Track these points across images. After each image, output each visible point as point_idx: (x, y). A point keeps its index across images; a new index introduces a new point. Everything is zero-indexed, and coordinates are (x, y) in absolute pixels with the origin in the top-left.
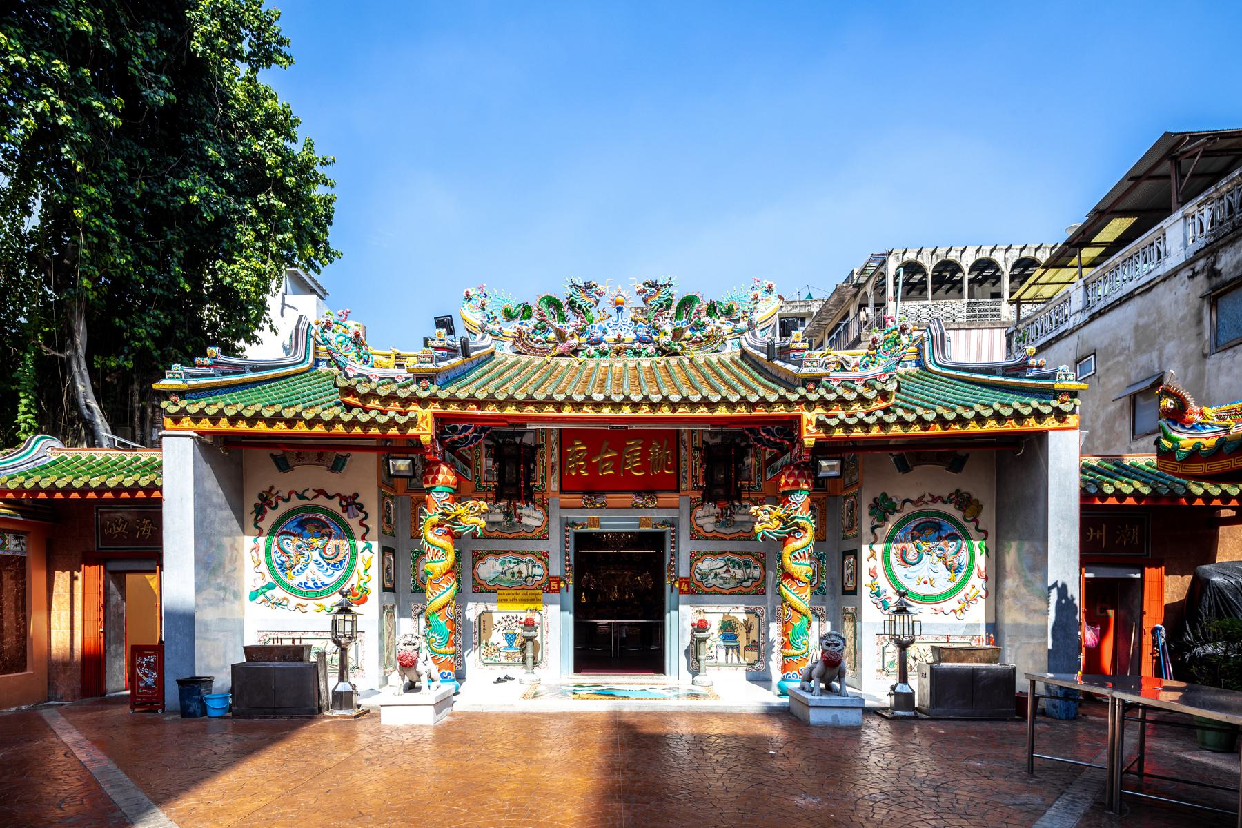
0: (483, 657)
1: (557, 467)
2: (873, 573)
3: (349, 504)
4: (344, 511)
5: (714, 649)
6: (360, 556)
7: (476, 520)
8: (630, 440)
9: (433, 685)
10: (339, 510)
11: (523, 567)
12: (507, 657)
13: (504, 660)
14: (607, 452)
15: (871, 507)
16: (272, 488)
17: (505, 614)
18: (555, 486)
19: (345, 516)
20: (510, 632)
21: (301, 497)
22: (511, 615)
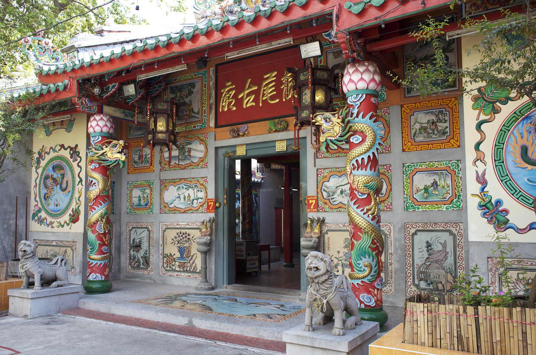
0: (165, 265)
1: (214, 107)
2: (482, 181)
3: (74, 153)
4: (71, 158)
5: (340, 268)
6: (77, 187)
7: (119, 155)
8: (266, 74)
9: (352, 320)
10: (68, 156)
11: (191, 191)
12: (179, 266)
13: (178, 269)
14: (250, 87)
15: (475, 99)
16: (43, 146)
17: (179, 231)
18: (212, 124)
19: (71, 160)
20: (182, 245)
21: (55, 151)
22: (184, 231)
